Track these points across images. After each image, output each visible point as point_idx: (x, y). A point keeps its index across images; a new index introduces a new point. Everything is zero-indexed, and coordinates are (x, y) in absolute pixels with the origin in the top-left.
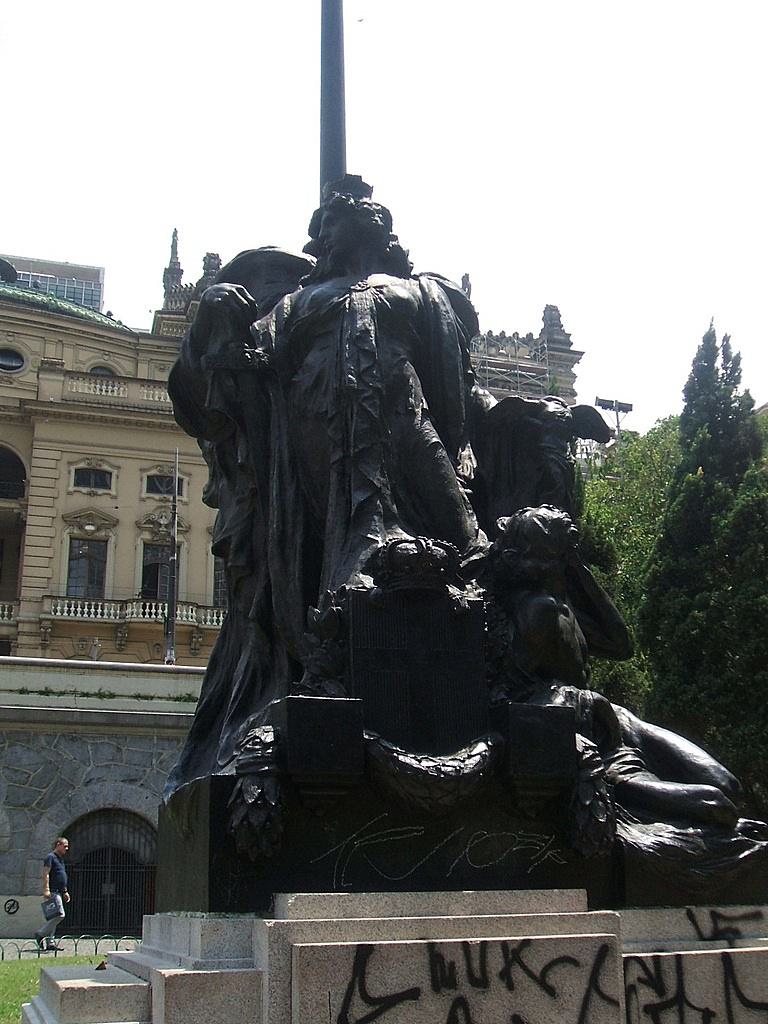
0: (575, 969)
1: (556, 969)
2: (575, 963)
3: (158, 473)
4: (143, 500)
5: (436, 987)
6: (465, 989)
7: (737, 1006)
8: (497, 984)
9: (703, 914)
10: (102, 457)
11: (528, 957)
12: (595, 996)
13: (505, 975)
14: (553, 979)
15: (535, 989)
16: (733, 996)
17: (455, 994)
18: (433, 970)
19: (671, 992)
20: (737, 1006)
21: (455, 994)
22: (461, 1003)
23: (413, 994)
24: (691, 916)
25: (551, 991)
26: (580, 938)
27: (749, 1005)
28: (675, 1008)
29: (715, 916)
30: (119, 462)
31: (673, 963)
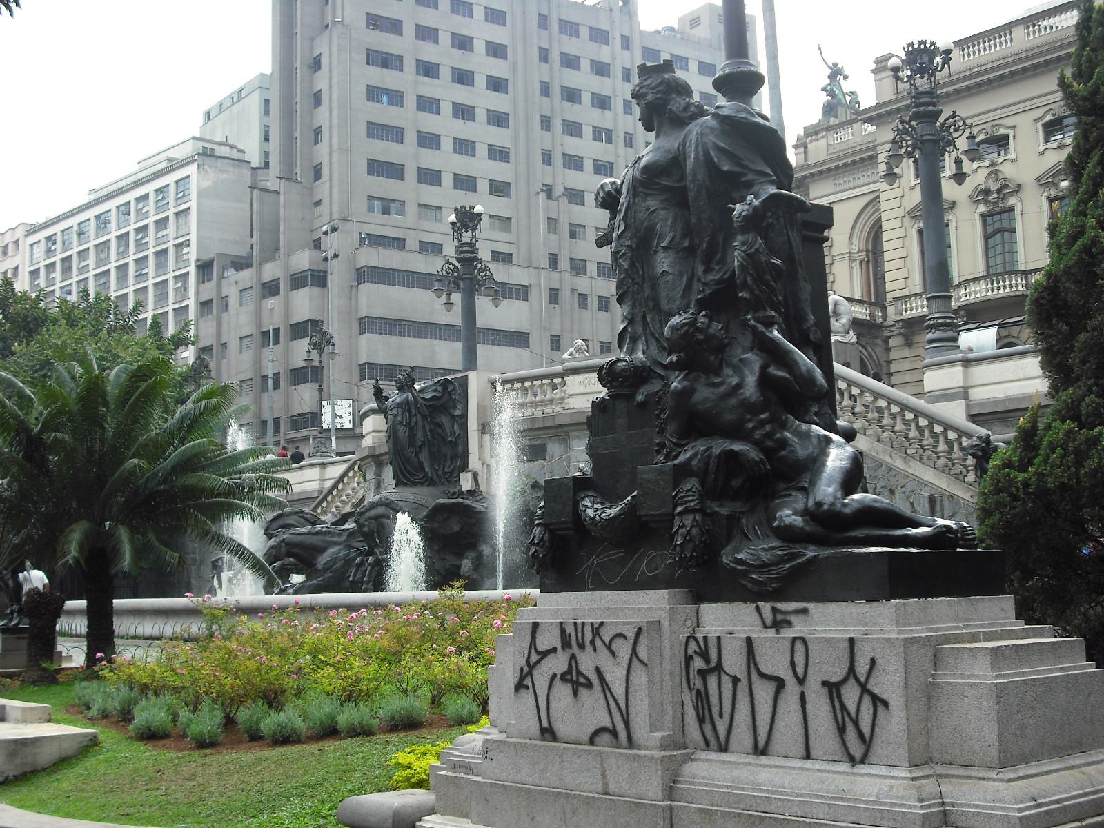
0: (625, 642)
1: (615, 640)
2: (625, 638)
3: (1052, 118)
4: (1041, 154)
5: (563, 648)
6: (575, 649)
7: (754, 676)
8: (589, 648)
9: (766, 607)
10: (996, 122)
11: (603, 631)
12: (634, 659)
13: (592, 642)
14: (614, 647)
15: (606, 651)
16: (753, 669)
17: (571, 652)
18: (562, 638)
19: (713, 664)
20: (754, 676)
21: (571, 652)
22: (573, 657)
23: (554, 650)
24: (758, 609)
25: (613, 654)
26: (1028, 645)
27: (763, 676)
28: (716, 673)
29: (774, 610)
30: (1009, 122)
31: (715, 641)
